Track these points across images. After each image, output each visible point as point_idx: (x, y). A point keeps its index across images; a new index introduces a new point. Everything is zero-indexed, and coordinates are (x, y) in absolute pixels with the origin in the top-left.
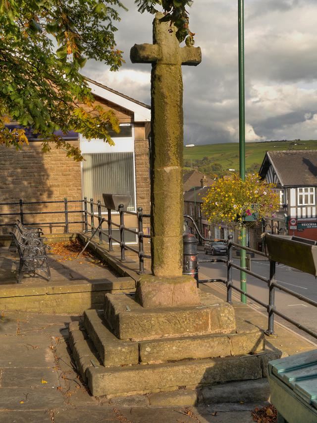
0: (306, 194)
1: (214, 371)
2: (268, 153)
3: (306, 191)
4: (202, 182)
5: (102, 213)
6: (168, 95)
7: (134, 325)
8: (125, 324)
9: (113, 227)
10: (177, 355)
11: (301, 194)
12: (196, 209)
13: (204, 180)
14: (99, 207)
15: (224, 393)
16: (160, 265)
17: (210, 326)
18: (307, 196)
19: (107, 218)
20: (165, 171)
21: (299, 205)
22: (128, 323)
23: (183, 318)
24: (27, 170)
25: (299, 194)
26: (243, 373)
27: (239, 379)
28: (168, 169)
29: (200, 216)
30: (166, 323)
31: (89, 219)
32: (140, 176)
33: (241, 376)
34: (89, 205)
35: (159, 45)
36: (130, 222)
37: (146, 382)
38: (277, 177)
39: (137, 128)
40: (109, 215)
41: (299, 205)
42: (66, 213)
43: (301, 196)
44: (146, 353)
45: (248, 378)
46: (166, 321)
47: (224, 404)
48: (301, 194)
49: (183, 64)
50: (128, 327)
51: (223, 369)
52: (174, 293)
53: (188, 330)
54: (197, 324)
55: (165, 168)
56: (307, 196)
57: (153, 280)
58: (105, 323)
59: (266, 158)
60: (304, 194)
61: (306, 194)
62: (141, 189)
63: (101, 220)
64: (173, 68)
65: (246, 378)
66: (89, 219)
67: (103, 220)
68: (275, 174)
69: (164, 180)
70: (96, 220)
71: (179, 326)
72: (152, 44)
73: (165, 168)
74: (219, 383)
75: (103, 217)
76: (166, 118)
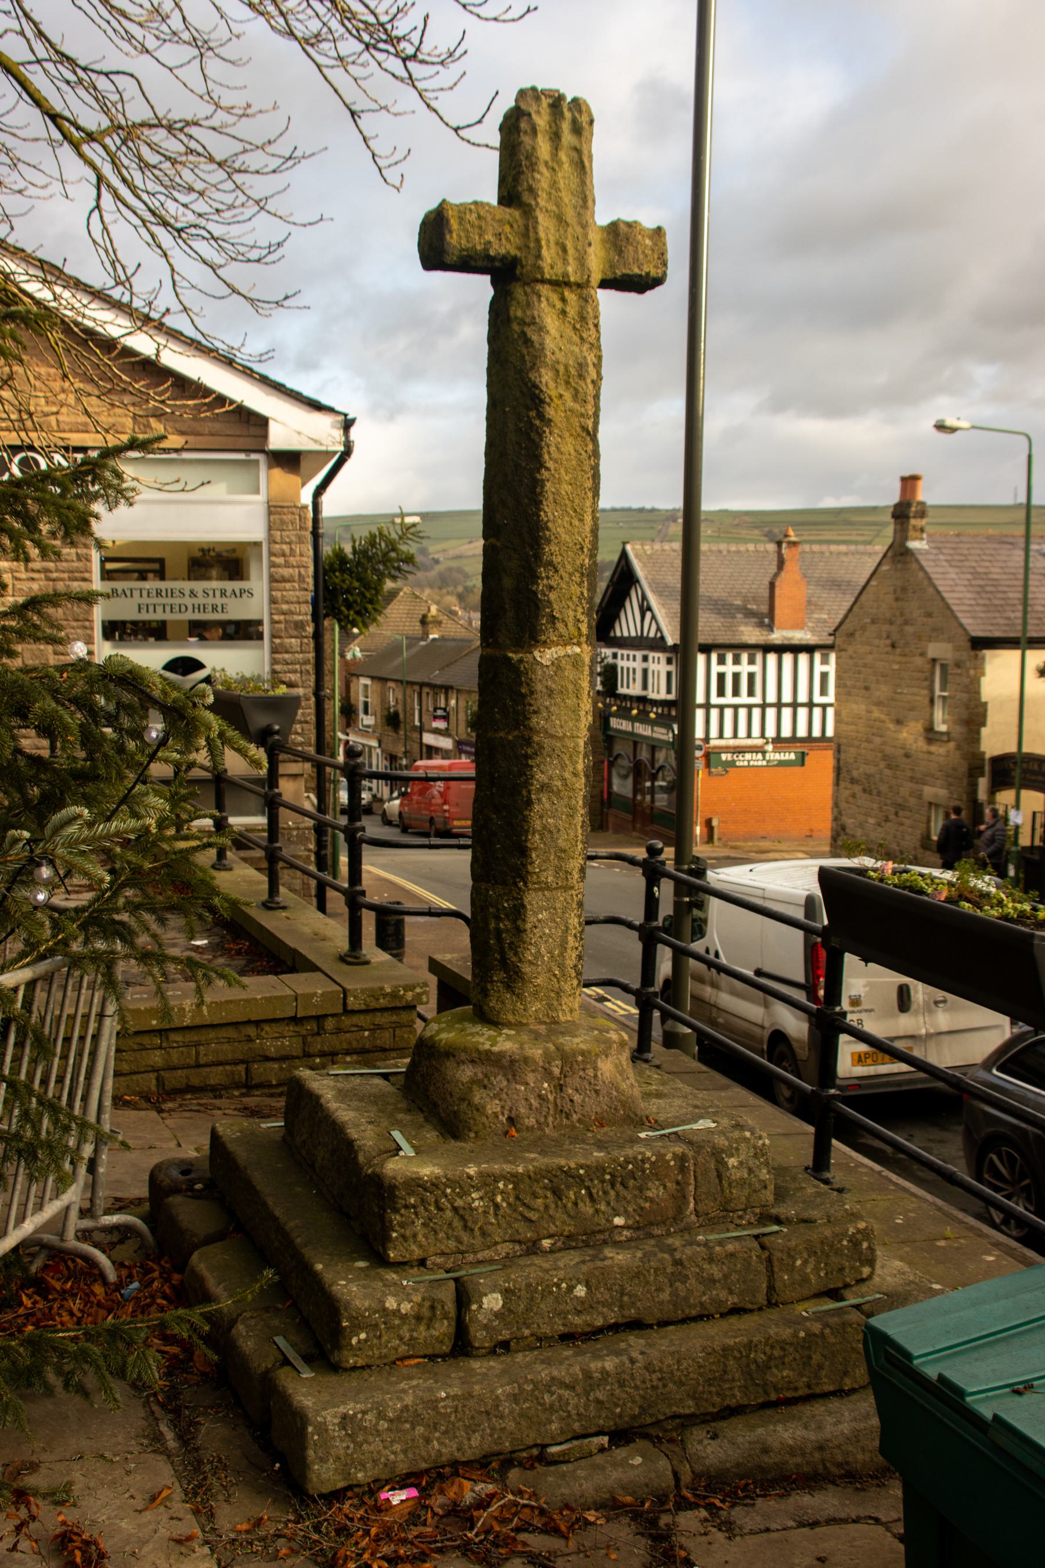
0: (737, 669)
2: (628, 547)
3: (737, 661)
4: (423, 621)
6: (554, 393)
9: (288, 820)
11: (722, 669)
12: (409, 700)
13: (430, 619)
18: (736, 677)
28: (546, 656)
29: (417, 723)
32: (282, 617)
35: (528, 212)
38: (653, 617)
39: (277, 472)
43: (721, 677)
48: (722, 669)
49: (605, 284)
52: (561, 1088)
56: (736, 677)
59: (623, 563)
60: (729, 669)
61: (737, 669)
62: (286, 656)
64: (570, 296)
68: (649, 609)
72: (494, 201)
73: (536, 654)
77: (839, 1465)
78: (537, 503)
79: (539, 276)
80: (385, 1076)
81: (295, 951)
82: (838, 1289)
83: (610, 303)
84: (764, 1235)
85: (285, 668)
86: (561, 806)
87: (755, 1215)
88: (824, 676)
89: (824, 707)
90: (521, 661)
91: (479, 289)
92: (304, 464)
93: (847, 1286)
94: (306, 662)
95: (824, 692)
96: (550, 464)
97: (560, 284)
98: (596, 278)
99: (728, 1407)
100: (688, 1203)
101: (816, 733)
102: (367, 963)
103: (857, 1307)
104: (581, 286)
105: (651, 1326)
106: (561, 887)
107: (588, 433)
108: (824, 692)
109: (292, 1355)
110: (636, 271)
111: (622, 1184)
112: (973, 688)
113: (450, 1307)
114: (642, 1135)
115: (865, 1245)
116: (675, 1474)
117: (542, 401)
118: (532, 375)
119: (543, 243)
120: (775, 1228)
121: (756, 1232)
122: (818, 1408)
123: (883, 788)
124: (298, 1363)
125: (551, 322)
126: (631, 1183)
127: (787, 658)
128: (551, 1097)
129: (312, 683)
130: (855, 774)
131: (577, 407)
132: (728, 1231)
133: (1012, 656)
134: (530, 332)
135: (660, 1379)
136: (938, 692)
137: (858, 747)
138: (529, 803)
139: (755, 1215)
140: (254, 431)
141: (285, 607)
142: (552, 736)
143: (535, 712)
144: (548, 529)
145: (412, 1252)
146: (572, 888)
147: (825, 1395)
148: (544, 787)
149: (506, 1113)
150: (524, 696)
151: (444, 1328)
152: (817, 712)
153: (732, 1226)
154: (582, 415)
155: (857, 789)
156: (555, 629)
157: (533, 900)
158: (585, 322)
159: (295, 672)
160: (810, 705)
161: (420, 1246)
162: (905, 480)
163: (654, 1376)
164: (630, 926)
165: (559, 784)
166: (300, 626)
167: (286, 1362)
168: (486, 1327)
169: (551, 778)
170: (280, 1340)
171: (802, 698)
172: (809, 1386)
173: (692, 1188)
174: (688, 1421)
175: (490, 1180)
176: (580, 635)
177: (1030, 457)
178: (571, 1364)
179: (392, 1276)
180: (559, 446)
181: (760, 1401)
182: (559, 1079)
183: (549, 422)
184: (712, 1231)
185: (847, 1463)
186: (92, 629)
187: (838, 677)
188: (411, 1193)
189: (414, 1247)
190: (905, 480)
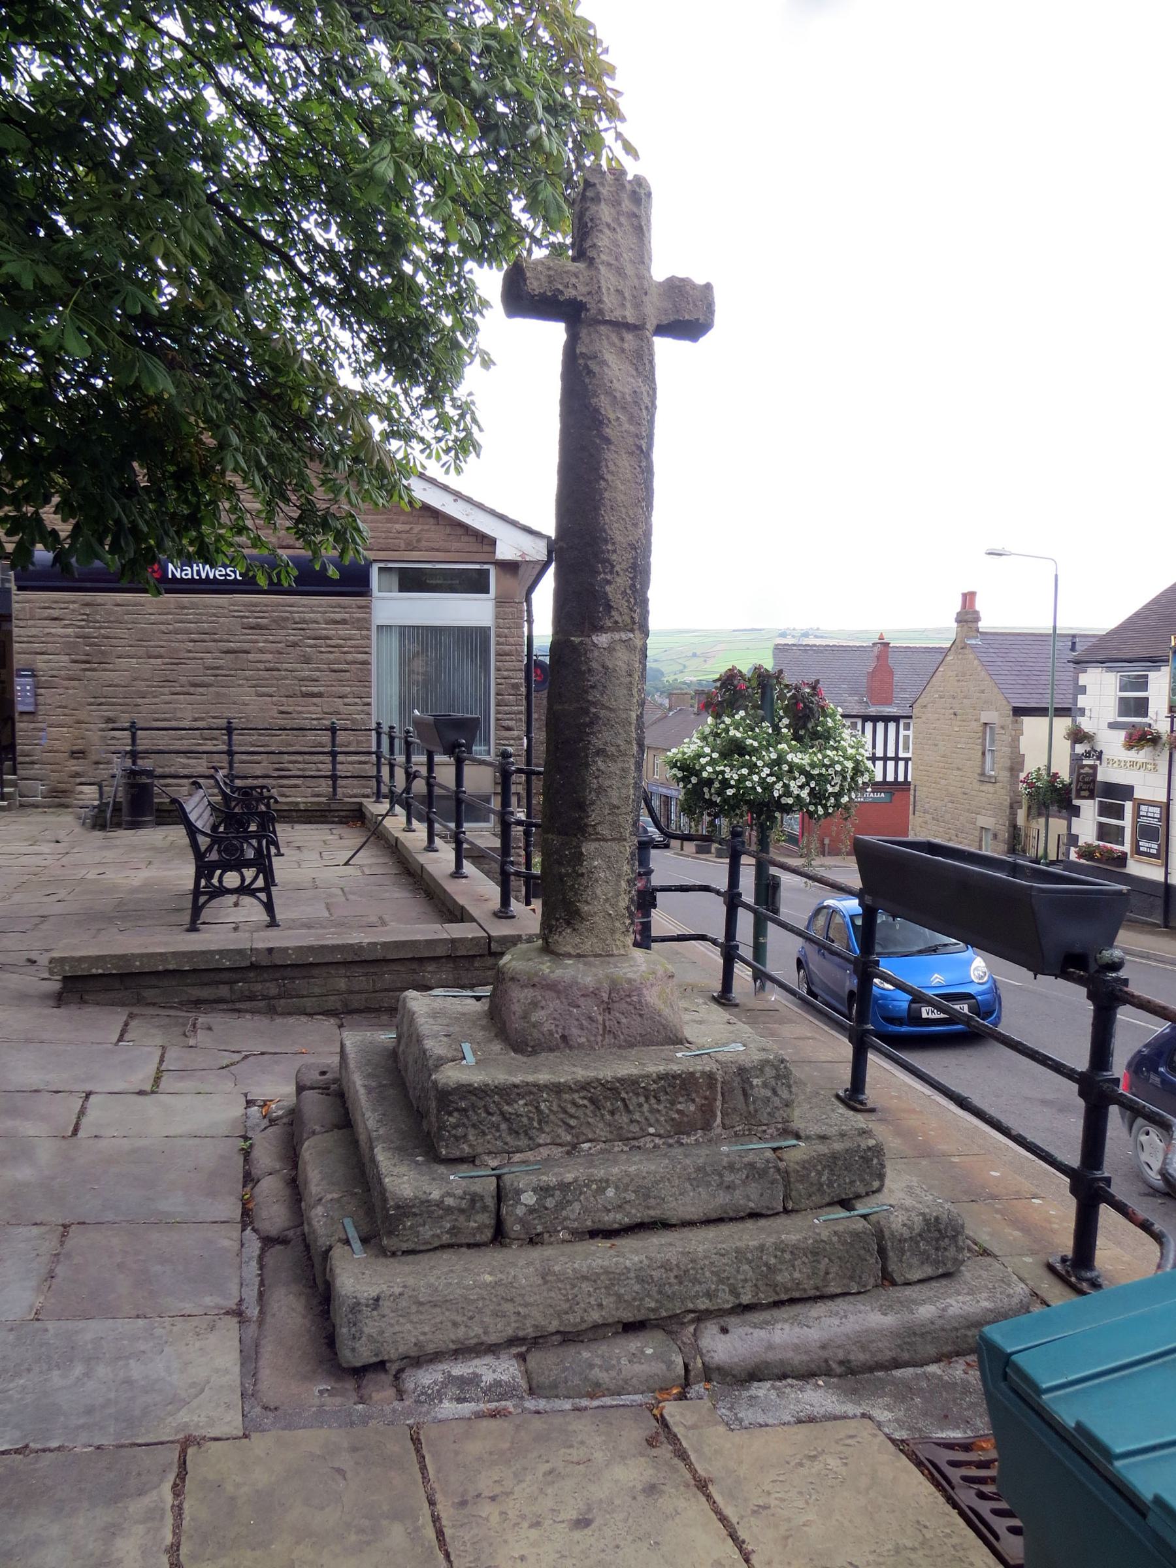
1: (738, 1272)
5: (414, 758)
6: (612, 416)
7: (484, 1115)
8: (456, 1114)
10: (619, 1216)
14: (408, 744)
15: (770, 1347)
16: (568, 923)
17: (719, 1114)
19: (424, 771)
20: (595, 645)
21: (901, 755)
22: (465, 1110)
23: (637, 1095)
24: (346, 700)
25: (902, 732)
26: (827, 1273)
27: (812, 1293)
30: (586, 1106)
31: (385, 771)
33: (820, 1284)
34: (385, 740)
35: (591, 262)
36: (479, 779)
37: (519, 1313)
40: (430, 765)
41: (901, 755)
42: (334, 754)
44: (520, 1211)
45: (839, 1291)
46: (586, 1102)
47: (768, 1384)
48: (907, 733)
50: (465, 1120)
51: (766, 1264)
53: (652, 1130)
54: (679, 1112)
55: (594, 638)
57: (626, 1219)
58: (628, 153)
63: (410, 776)
64: (629, 337)
65: (833, 1289)
66: (385, 771)
67: (416, 775)
69: (590, 670)
70: (400, 774)
71: (625, 1119)
74: (744, 1309)
75: (415, 768)
76: (603, 483)
77: (841, 1363)
78: (596, 509)
79: (600, 318)
80: (478, 998)
81: (463, 908)
82: (850, 1199)
83: (665, 349)
84: (780, 1148)
85: (505, 716)
86: (614, 767)
87: (778, 1130)
88: (907, 738)
89: (907, 760)
90: (581, 643)
91: (554, 333)
92: (521, 571)
93: (858, 1197)
94: (520, 713)
95: (906, 749)
96: (609, 477)
97: (620, 326)
98: (651, 324)
99: (740, 1305)
100: (715, 1116)
101: (901, 778)
102: (513, 917)
103: (865, 1216)
104: (636, 328)
105: (674, 1226)
106: (614, 839)
107: (642, 451)
108: (906, 749)
109: (352, 1234)
110: (687, 317)
111: (655, 1097)
112: (1015, 743)
113: (490, 1202)
114: (679, 1055)
115: (875, 1161)
116: (686, 1366)
117: (601, 422)
118: (594, 401)
119: (604, 290)
120: (794, 1142)
121: (775, 1145)
122: (818, 1310)
123: (948, 816)
124: (357, 1245)
125: (610, 357)
126: (663, 1098)
127: (880, 726)
128: (600, 1018)
129: (524, 729)
130: (927, 806)
131: (632, 428)
132: (751, 1142)
133: (1042, 722)
134: (592, 365)
135: (676, 1277)
136: (988, 748)
137: (929, 787)
138: (587, 765)
139: (778, 1130)
140: (486, 548)
141: (506, 673)
142: (608, 708)
143: (592, 687)
144: (605, 531)
145: (462, 1150)
146: (625, 840)
147: (833, 1297)
148: (600, 752)
149: (560, 1031)
150: (583, 673)
151: (486, 1219)
152: (901, 764)
153: (755, 1139)
154: (637, 436)
155: (928, 816)
156: (611, 617)
157: (588, 848)
158: (643, 365)
159: (512, 719)
160: (897, 759)
161: (470, 1146)
162: (965, 596)
163: (672, 1275)
164: (718, 892)
165: (613, 749)
166: (516, 686)
167: (347, 1242)
168: (521, 1221)
169: (606, 744)
170: (348, 1222)
171: (891, 754)
172: (817, 1288)
173: (719, 1103)
174: (702, 1316)
175: (535, 1090)
176: (634, 623)
177: (1056, 576)
178: (599, 1256)
179: (442, 1169)
180: (618, 463)
181: (771, 1300)
182: (608, 1003)
183: (608, 441)
184: (736, 1143)
185: (849, 1361)
186: (370, 687)
187: (915, 737)
188: (463, 1098)
189: (465, 1146)
190: (965, 596)
